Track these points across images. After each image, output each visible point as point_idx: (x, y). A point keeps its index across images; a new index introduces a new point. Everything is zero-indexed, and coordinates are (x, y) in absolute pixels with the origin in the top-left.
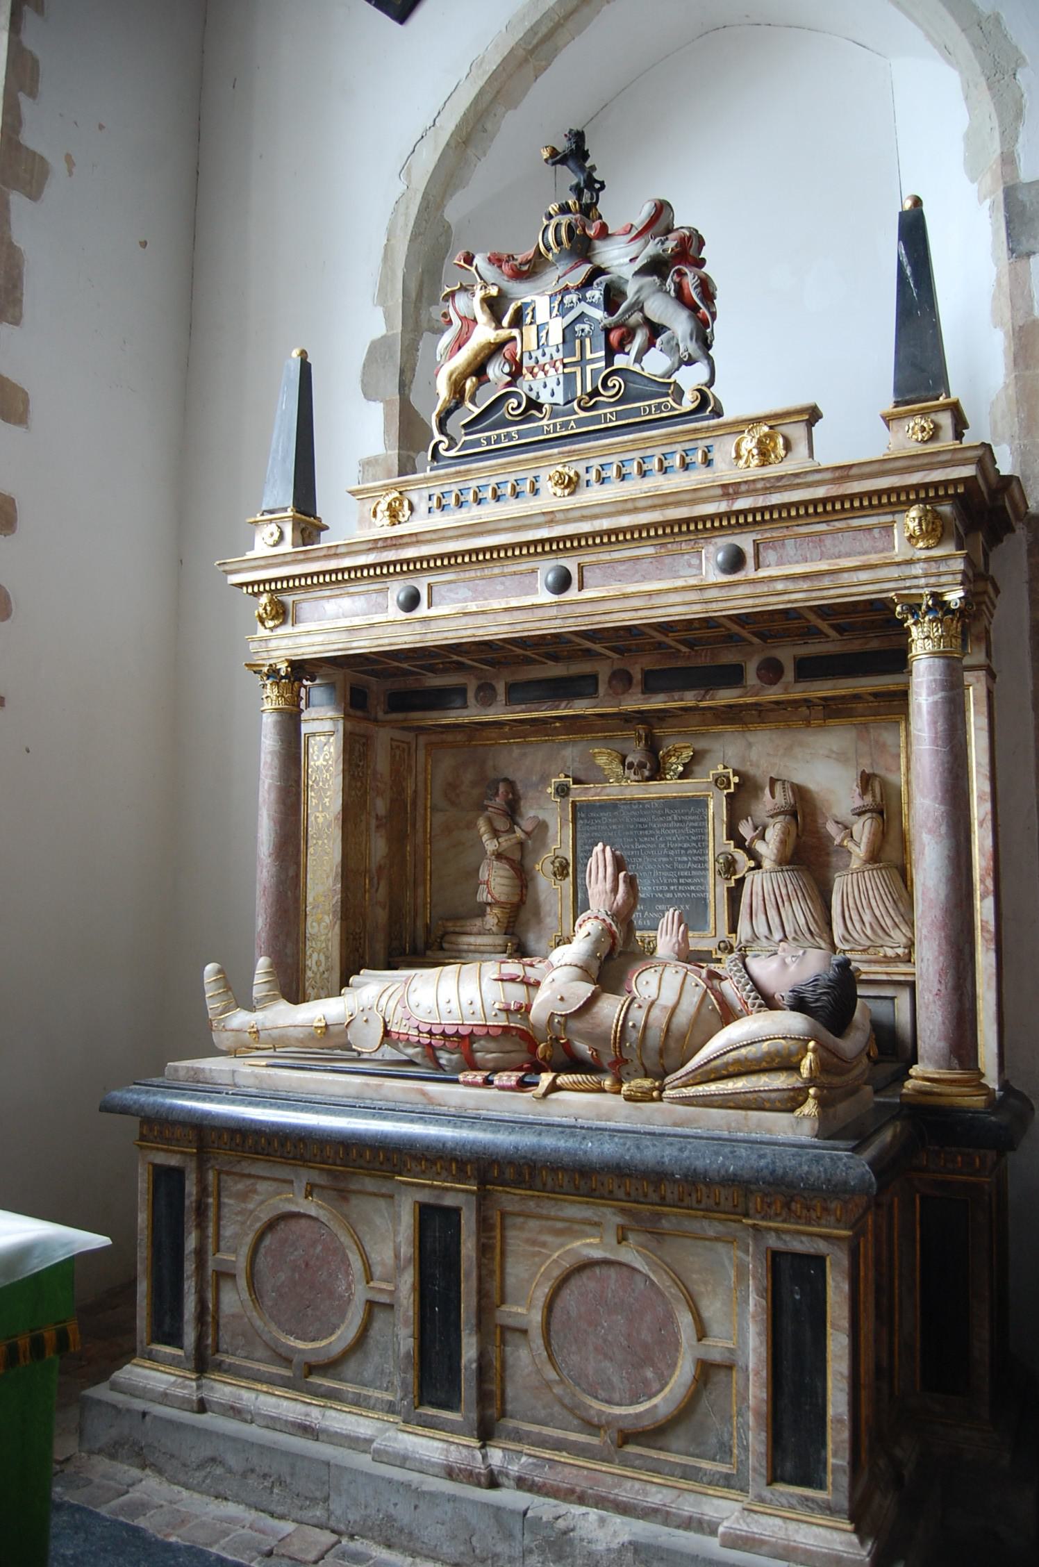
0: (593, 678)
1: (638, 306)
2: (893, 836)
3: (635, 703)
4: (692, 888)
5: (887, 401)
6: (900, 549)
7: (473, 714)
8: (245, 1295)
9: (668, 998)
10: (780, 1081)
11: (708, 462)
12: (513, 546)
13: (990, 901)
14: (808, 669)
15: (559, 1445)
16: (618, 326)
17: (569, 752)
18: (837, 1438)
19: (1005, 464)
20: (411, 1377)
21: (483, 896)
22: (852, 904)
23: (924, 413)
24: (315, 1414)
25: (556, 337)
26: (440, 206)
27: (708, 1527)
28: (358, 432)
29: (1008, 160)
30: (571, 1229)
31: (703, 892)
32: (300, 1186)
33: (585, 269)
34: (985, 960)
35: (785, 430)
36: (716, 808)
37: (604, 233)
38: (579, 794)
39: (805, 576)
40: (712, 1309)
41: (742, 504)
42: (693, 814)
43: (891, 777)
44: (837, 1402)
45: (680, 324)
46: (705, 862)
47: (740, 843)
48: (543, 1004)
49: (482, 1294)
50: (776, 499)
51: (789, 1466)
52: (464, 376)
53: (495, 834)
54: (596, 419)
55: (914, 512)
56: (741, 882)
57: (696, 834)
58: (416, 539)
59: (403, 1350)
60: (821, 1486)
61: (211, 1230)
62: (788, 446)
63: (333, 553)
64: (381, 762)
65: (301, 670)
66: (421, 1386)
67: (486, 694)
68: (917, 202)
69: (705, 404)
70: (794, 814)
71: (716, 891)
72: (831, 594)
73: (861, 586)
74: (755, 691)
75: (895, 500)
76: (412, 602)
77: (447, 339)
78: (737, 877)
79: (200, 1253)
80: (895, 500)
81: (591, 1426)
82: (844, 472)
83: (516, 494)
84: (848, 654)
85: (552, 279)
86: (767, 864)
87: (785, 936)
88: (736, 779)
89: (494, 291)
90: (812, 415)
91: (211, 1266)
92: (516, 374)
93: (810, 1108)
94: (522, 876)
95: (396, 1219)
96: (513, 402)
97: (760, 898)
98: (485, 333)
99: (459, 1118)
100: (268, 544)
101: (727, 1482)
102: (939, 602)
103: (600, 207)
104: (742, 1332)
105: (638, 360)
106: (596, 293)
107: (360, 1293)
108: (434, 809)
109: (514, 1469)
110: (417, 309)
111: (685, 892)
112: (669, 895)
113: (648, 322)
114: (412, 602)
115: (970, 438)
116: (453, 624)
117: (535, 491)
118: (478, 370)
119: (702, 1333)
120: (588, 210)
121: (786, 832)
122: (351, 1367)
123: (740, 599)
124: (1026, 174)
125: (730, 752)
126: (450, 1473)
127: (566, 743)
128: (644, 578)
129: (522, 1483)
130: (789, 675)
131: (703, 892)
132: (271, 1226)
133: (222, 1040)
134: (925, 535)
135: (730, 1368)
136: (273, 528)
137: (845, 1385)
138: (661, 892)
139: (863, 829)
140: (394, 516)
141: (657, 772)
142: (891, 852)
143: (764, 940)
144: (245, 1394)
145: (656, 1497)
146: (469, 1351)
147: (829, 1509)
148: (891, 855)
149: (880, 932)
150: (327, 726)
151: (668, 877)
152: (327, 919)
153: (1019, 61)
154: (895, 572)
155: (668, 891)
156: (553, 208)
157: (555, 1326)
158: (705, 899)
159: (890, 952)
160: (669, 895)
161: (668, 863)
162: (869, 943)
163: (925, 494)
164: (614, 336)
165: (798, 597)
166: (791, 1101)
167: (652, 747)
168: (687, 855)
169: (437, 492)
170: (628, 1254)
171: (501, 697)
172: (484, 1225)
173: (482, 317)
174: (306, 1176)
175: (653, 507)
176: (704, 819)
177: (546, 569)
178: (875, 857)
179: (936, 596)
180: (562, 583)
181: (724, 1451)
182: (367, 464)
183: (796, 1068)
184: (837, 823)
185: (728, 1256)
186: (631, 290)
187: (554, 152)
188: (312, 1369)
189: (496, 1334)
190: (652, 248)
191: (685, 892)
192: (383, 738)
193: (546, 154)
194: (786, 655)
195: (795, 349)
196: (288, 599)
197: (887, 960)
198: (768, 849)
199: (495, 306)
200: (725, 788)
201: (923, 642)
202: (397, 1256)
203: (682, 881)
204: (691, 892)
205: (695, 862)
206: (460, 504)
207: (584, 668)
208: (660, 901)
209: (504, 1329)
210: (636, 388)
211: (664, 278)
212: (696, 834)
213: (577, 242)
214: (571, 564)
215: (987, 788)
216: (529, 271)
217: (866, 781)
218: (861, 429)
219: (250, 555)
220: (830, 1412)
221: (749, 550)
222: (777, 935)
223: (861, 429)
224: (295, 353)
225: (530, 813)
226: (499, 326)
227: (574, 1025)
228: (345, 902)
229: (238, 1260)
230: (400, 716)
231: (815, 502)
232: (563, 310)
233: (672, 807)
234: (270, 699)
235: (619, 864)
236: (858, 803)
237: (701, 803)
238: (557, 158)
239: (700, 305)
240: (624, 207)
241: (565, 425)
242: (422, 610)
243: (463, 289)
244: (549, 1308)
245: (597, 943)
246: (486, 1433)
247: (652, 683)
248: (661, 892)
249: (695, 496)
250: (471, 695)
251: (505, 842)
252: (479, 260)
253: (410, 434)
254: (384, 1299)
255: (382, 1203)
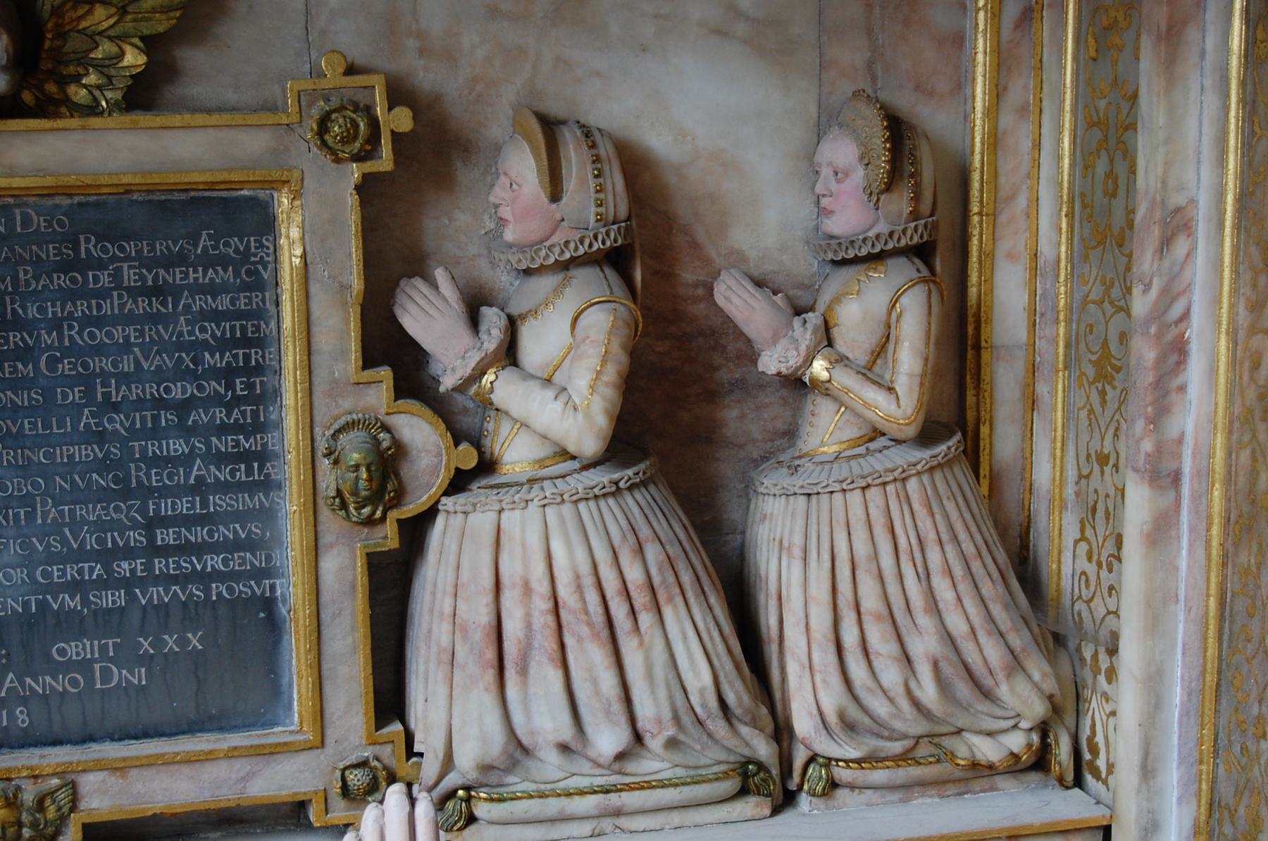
4: (214, 562)
22: (871, 602)
31: (261, 574)
36: (312, 234)
42: (208, 262)
46: (263, 456)
56: (416, 531)
57: (224, 344)
70: (616, 260)
78: (410, 509)
87: (638, 738)
88: (402, 120)
97: (542, 605)
111: (182, 579)
112: (112, 599)
131: (261, 574)
138: (75, 586)
143: (552, 758)
149: (963, 690)
151: (101, 526)
155: (107, 583)
158: (269, 604)
159: (989, 751)
160: (112, 599)
161: (103, 466)
162: (918, 727)
168: (187, 432)
176: (257, 278)
184: (759, 283)
191: (182, 579)
197: (980, 771)
200: (357, 158)
203: (166, 537)
204: (205, 578)
205: (220, 459)
208: (70, 625)
212: (224, 344)
222: (607, 739)
233: (112, 233)
236: (850, 217)
237: (236, 216)
248: (75, 586)
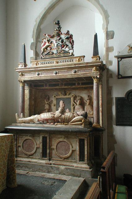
0: (43, 85)
1: (65, 43)
2: (91, 102)
3: (63, 87)
5: (92, 56)
6: (93, 72)
7: (45, 88)
8: (22, 148)
9: (69, 115)
10: (80, 122)
11: (73, 61)
12: (51, 69)
13: (101, 108)
14: (83, 84)
15: (58, 160)
16: (63, 45)
17: (55, 92)
18: (86, 158)
19: (104, 63)
20: (42, 155)
21: (45, 108)
23: (96, 57)
24: (30, 160)
25: (56, 45)
26: (40, 26)
27: (73, 166)
28: (30, 54)
29: (107, 28)
30: (59, 138)
32: (29, 136)
33: (59, 37)
34: (101, 114)
35: (81, 58)
36: (72, 99)
37: (61, 34)
38: (57, 97)
39: (83, 74)
40: (73, 145)
41: (76, 66)
43: (91, 96)
44: (86, 153)
45: (70, 45)
47: (75, 102)
48: (56, 116)
49: (50, 145)
50: (80, 66)
51: (81, 160)
52: (45, 49)
53: (47, 101)
54: (60, 55)
55: (94, 68)
56: (75, 107)
58: (39, 67)
59: (41, 152)
60: (84, 161)
61: (18, 141)
62: (81, 60)
63: (29, 68)
64: (33, 93)
65: (25, 81)
66: (43, 155)
67: (46, 86)
68: (96, 34)
69: (73, 54)
71: (72, 108)
72: (85, 76)
73: (89, 75)
74: (76, 86)
75: (92, 66)
76: (39, 75)
77: (43, 44)
79: (16, 144)
80: (92, 66)
81: (61, 158)
82: (87, 63)
83: (51, 63)
84: (86, 83)
85: (56, 38)
86: (78, 105)
89: (48, 39)
90: (84, 56)
91: (18, 145)
92: (51, 49)
93: (83, 125)
94: (50, 106)
95: (40, 138)
96: (51, 52)
98: (47, 44)
99: (47, 127)
100: (21, 66)
101: (75, 162)
102: (97, 77)
103: (61, 30)
104: (76, 147)
105: (65, 49)
106: (60, 41)
107: (36, 147)
108: (39, 98)
109: (53, 163)
110: (37, 39)
113: (66, 44)
114: (39, 75)
115: (101, 60)
116: (44, 77)
117: (53, 63)
118: (46, 48)
119: (72, 147)
120: (60, 31)
121: (80, 101)
122: (34, 155)
123: (76, 76)
124: (109, 30)
125: (74, 93)
126: (46, 164)
127: (55, 92)
128: (65, 73)
129: (54, 164)
130: (80, 85)
132: (25, 140)
133: (18, 122)
134: (95, 70)
135: (75, 151)
136: (21, 65)
137: (87, 151)
139: (88, 101)
140: (36, 65)
141: (66, 95)
142: (91, 104)
144: (22, 159)
145: (68, 164)
146: (48, 151)
147: (85, 163)
148: (91, 104)
150: (27, 88)
152: (27, 110)
153: (109, 16)
154: (92, 74)
156: (55, 30)
157: (57, 148)
163: (96, 66)
164: (62, 46)
165: (82, 76)
166: (81, 124)
167: (65, 92)
169: (42, 62)
170: (65, 140)
171: (48, 86)
172: (50, 138)
173: (47, 42)
174: (29, 135)
175: (67, 66)
177: (55, 72)
178: (89, 104)
179: (96, 77)
180: (56, 73)
181: (75, 159)
182: (31, 58)
183: (82, 121)
185: (75, 140)
186: (64, 41)
187: (56, 23)
188: (30, 155)
189: (51, 149)
190: (67, 36)
192: (34, 90)
193: (55, 23)
194: (80, 82)
195: (82, 49)
196: (23, 73)
197: (91, 115)
198: (78, 103)
199: (48, 41)
201: (95, 81)
202: (40, 142)
206: (44, 64)
207: (42, 84)
209: (52, 149)
210: (65, 52)
211: (68, 40)
213: (54, 28)
214: (57, 71)
215: (101, 96)
216: (53, 37)
217: (89, 96)
218: (89, 58)
219: (18, 68)
220: (85, 154)
221: (77, 71)
223: (89, 58)
224: (23, 44)
225: (51, 99)
226: (49, 43)
227: (59, 118)
228: (29, 108)
229: (21, 144)
230: (36, 87)
231: (84, 66)
232: (57, 42)
234: (21, 85)
235: (63, 103)
238: (56, 24)
239: (72, 43)
240: (64, 31)
241: (57, 56)
242: (40, 76)
243: (45, 38)
244: (57, 146)
245: (61, 110)
246: (50, 160)
247: (65, 85)
249: (71, 65)
250: (44, 85)
251: (48, 102)
252: (46, 35)
253: (37, 54)
254: (38, 147)
255: (38, 137)
